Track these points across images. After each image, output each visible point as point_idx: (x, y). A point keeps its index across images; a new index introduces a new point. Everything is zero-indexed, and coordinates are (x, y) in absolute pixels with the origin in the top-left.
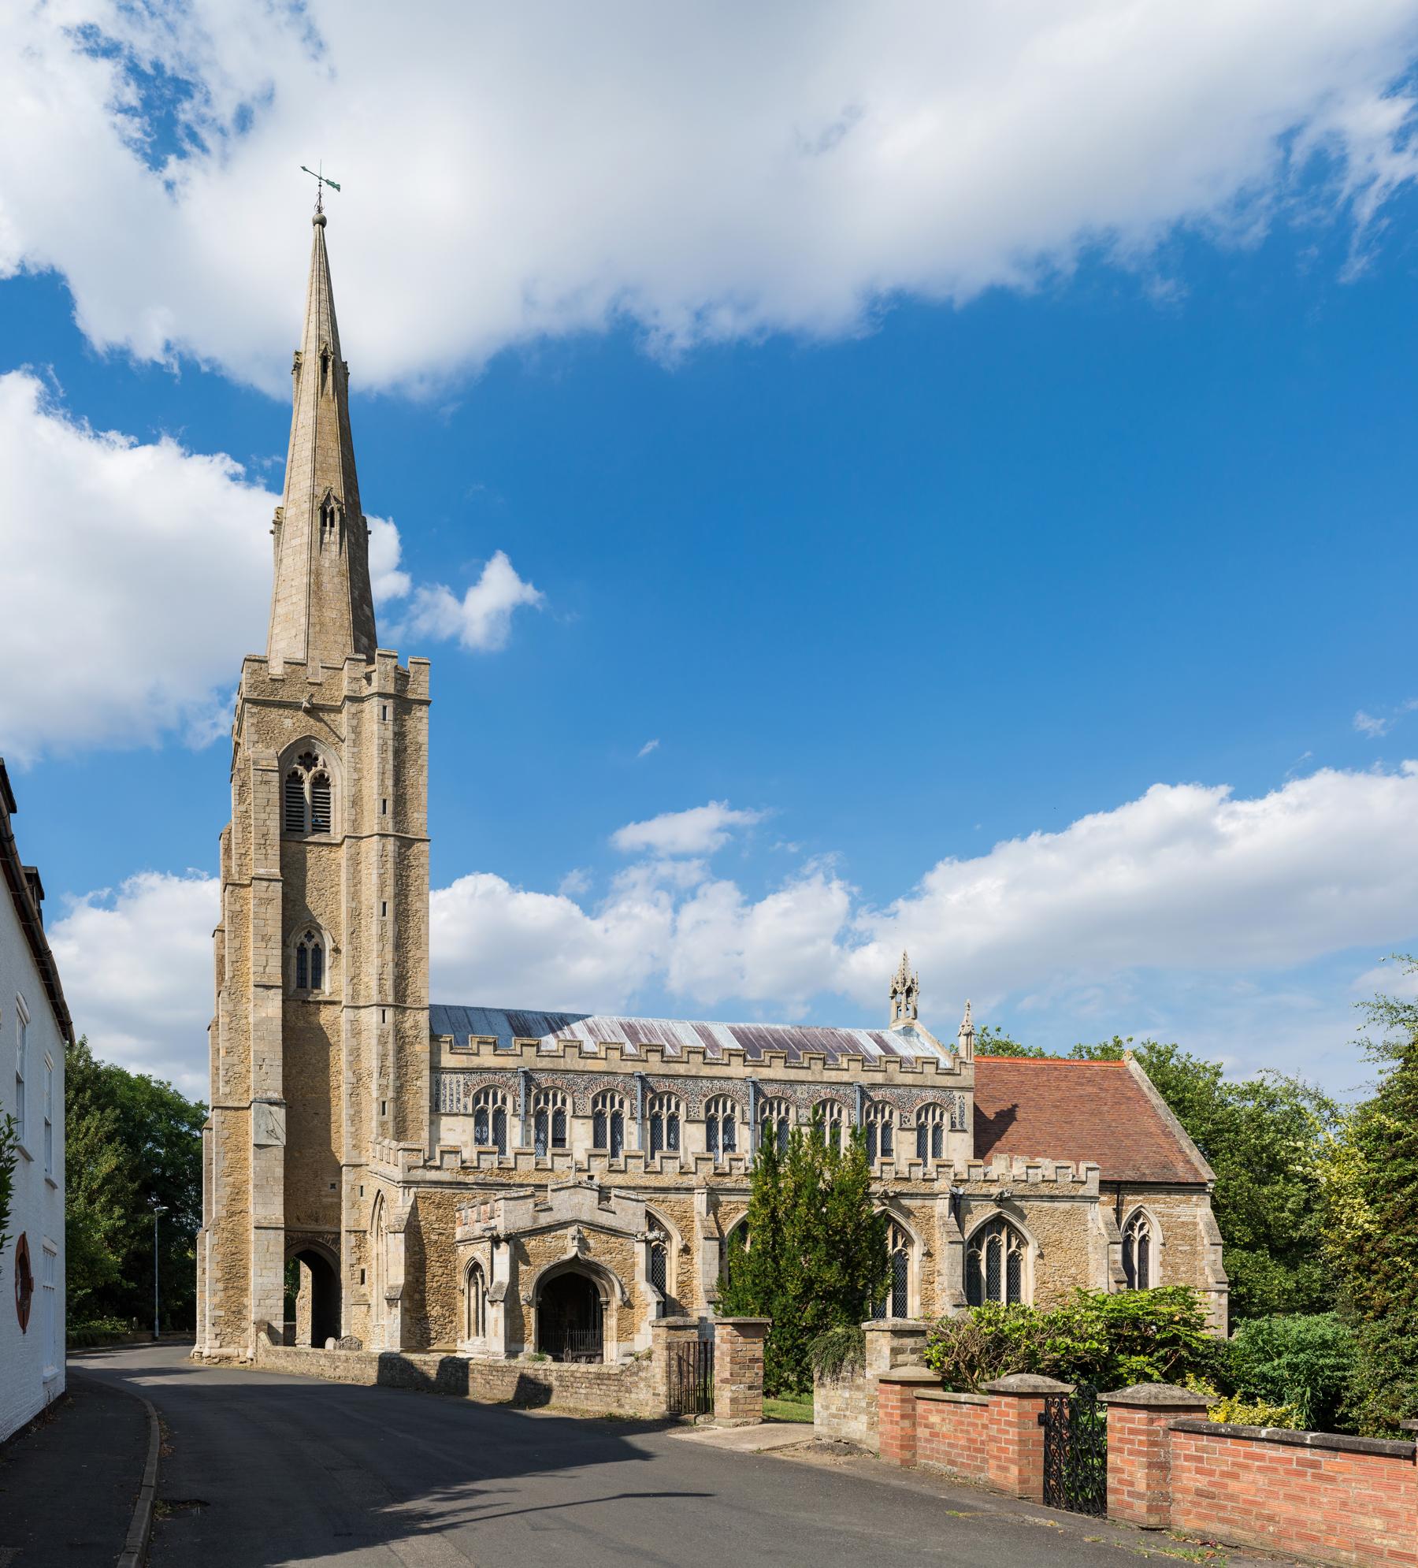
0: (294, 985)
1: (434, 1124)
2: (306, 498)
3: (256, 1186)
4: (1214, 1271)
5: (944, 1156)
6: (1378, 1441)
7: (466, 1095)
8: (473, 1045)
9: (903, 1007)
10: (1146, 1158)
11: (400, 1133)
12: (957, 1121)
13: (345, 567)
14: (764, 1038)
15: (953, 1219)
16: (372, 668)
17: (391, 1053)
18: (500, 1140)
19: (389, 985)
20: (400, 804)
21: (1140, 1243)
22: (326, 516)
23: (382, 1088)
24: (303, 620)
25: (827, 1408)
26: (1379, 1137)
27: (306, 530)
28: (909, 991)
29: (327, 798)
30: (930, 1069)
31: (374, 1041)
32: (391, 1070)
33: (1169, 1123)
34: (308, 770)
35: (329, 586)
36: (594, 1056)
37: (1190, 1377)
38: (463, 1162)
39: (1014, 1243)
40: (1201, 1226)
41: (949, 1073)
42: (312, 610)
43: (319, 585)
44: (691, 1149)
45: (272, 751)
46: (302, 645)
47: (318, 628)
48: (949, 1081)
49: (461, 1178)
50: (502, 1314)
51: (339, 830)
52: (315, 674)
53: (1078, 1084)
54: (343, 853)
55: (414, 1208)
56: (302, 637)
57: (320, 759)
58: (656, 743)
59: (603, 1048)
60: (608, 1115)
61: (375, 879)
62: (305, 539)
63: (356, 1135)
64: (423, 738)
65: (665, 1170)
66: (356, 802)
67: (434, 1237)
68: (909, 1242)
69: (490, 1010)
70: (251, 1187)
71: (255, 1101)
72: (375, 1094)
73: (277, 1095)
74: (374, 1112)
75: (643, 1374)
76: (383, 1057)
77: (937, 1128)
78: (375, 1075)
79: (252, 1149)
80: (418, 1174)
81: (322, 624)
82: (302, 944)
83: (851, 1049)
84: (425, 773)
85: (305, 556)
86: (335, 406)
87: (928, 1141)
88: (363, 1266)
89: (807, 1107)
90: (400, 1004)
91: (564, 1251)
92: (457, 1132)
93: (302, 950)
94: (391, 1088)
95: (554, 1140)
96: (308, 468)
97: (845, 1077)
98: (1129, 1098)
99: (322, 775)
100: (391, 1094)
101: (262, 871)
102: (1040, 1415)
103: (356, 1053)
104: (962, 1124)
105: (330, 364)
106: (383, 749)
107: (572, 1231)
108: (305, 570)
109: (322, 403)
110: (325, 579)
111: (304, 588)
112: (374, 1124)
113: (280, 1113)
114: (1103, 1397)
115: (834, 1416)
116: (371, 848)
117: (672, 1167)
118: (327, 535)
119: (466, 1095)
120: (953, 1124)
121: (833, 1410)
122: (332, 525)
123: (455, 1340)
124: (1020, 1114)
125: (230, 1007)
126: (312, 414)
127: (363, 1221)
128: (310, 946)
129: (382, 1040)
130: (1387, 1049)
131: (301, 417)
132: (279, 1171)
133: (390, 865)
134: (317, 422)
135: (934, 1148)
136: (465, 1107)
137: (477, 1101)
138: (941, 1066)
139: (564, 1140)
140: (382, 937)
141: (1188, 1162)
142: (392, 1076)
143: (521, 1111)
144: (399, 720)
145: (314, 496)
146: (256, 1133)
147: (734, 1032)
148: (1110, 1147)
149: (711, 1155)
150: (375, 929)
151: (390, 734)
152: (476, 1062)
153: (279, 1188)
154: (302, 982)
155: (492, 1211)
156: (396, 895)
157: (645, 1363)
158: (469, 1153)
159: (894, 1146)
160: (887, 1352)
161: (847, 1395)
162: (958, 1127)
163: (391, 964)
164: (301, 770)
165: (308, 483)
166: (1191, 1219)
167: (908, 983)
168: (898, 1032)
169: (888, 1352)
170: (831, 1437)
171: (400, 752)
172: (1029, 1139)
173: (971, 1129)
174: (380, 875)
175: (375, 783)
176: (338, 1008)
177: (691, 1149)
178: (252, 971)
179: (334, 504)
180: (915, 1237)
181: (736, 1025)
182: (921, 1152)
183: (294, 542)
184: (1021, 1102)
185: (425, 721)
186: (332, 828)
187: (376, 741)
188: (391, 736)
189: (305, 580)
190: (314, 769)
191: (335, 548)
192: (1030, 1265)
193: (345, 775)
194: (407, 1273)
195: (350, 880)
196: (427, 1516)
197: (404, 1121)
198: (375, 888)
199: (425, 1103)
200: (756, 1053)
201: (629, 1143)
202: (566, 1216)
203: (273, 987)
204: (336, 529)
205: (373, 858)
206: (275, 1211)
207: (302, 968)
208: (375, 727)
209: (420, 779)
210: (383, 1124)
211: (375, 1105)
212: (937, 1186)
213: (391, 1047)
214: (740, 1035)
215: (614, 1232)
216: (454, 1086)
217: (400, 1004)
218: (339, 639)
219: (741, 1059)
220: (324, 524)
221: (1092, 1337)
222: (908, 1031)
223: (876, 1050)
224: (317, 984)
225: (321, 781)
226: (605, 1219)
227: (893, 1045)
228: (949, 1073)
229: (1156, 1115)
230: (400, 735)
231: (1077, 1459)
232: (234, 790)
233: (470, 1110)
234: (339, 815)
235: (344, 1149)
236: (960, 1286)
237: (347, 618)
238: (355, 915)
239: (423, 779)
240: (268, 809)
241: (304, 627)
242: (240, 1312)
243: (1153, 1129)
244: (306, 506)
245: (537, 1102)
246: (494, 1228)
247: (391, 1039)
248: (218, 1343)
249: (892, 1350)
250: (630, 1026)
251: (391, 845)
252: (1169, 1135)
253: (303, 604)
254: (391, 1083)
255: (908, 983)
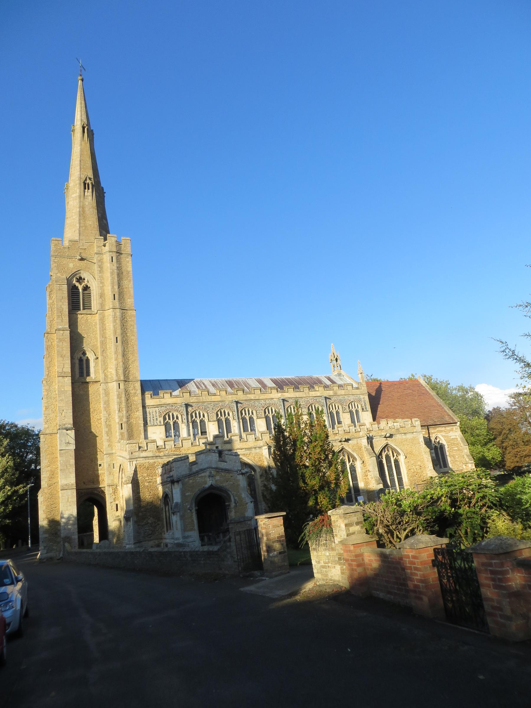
0: (77, 375)
1: (146, 431)
2: (77, 179)
3: (61, 470)
4: (467, 456)
5: (362, 422)
6: (153, 461)
7: (160, 417)
8: (161, 395)
9: (336, 366)
10: (434, 415)
11: (131, 436)
12: (364, 407)
13: (95, 204)
14: (285, 382)
15: (369, 447)
16: (106, 242)
17: (124, 401)
18: (177, 435)
19: (121, 371)
20: (120, 295)
21: (174, 425)
22: (85, 186)
23: (121, 418)
24: (78, 225)
25: (319, 562)
26: (482, 528)
27: (78, 191)
28: (336, 360)
29: (89, 295)
30: (350, 388)
31: (116, 397)
32: (124, 409)
33: (439, 401)
34: (81, 284)
35: (88, 212)
36: (215, 395)
37: (316, 388)
38: (157, 447)
39: (395, 455)
40: (459, 439)
41: (357, 388)
42: (81, 221)
43: (84, 211)
44: (346, 423)
45: (64, 277)
46: (78, 235)
47: (84, 228)
48: (358, 392)
49: (157, 454)
50: (178, 518)
51: (95, 308)
52: (83, 246)
53: (405, 389)
54: (97, 317)
55: (136, 471)
56: (77, 231)
57: (86, 279)
58: (242, 589)
59: (218, 391)
60: (224, 420)
61: (112, 327)
62: (78, 194)
63: (109, 440)
64: (130, 269)
65: (249, 440)
66: (102, 296)
67: (146, 484)
68: (354, 459)
69: (170, 380)
70: (59, 470)
71: (59, 429)
72: (117, 421)
73: (70, 426)
74: (117, 429)
75: (228, 550)
76: (120, 403)
77: (357, 411)
78: (117, 412)
79: (58, 452)
80: (136, 454)
81: (86, 227)
82: (81, 358)
83: (319, 382)
84: (132, 282)
85: (78, 201)
86: (88, 145)
87: (354, 418)
88: (117, 502)
89: (305, 408)
90: (126, 380)
91: (205, 483)
92: (157, 433)
93: (81, 360)
94: (125, 417)
95: (202, 433)
96: (78, 168)
97: (318, 394)
98: (423, 393)
99: (87, 286)
100: (125, 420)
101: (60, 327)
102: (433, 561)
103: (107, 403)
104: (366, 408)
105: (86, 129)
106: (112, 273)
107: (207, 473)
108: (78, 206)
109: (83, 143)
110: (86, 209)
111: (78, 213)
112: (118, 434)
113: (72, 433)
114: (57, 501)
115: (323, 567)
116: (109, 314)
117: (251, 438)
118: (86, 193)
119: (160, 417)
120: (363, 409)
121: (322, 564)
122: (88, 189)
123: (161, 534)
124: (428, 374)
125: (47, 388)
126: (79, 148)
127: (115, 480)
128: (84, 358)
129: (119, 397)
130: (165, 539)
131: (75, 149)
132: (73, 461)
133: (118, 321)
134: (81, 151)
135: (86, 368)
136: (160, 422)
137: (165, 419)
138: (354, 386)
139: (206, 432)
140: (116, 352)
141: (449, 415)
142: (124, 412)
143: (185, 421)
144: (119, 261)
145: (80, 178)
146: (60, 445)
147: (272, 380)
148: (421, 412)
149: (189, 438)
150: (113, 349)
151: (115, 267)
152: (163, 401)
153: (73, 470)
154: (81, 374)
155: (171, 469)
156: (122, 334)
157: (228, 544)
158: (160, 443)
159: (342, 420)
160: (343, 526)
161: (328, 554)
162: (365, 410)
163: (121, 363)
164: (77, 284)
165: (78, 173)
166: (455, 437)
167: (336, 357)
168: (336, 375)
169: (344, 527)
170: (323, 580)
171: (120, 274)
172: (392, 412)
173: (370, 410)
174: (114, 326)
175: (110, 288)
176: (99, 384)
177: (346, 423)
178: (56, 369)
179: (88, 181)
180: (357, 457)
181: (210, 379)
182: (353, 421)
183: (73, 196)
184: (72, 266)
185: (130, 262)
186: (92, 308)
187: (109, 271)
188: (116, 268)
189: (78, 210)
190: (83, 284)
191: (90, 198)
192: (403, 463)
193: (97, 285)
194: (88, 391)
195: (99, 326)
196: (303, 537)
197: (132, 431)
198: (112, 332)
199: (141, 422)
200: (282, 388)
201: (234, 430)
202: (205, 466)
203: (76, 341)
204: (90, 190)
205: (111, 319)
206: (72, 480)
207: (81, 368)
208: (109, 265)
209: (129, 285)
210: (122, 434)
211: (117, 426)
212: (361, 434)
213: (123, 399)
214: (275, 381)
215: (227, 471)
216: (154, 413)
217: (126, 380)
218: (93, 232)
219: (276, 390)
220: (85, 188)
221: (409, 388)
222: (339, 375)
223: (328, 383)
224: (88, 374)
225: (86, 288)
226: (223, 465)
227: (334, 380)
228: (357, 388)
229: (433, 399)
230: (119, 268)
231: (103, 331)
232: (48, 293)
233: (162, 423)
234: (95, 302)
235: (104, 447)
236: (378, 476)
237: (96, 224)
238: (103, 343)
239: (131, 285)
240: (62, 301)
241: (78, 228)
242: (56, 534)
243: (434, 404)
244: (78, 182)
245: (192, 417)
246: (172, 476)
247: (123, 395)
248: (45, 551)
249: (346, 525)
250: (230, 382)
251: (118, 312)
252: (440, 406)
253: (77, 219)
254: (124, 415)
255: (336, 357)
